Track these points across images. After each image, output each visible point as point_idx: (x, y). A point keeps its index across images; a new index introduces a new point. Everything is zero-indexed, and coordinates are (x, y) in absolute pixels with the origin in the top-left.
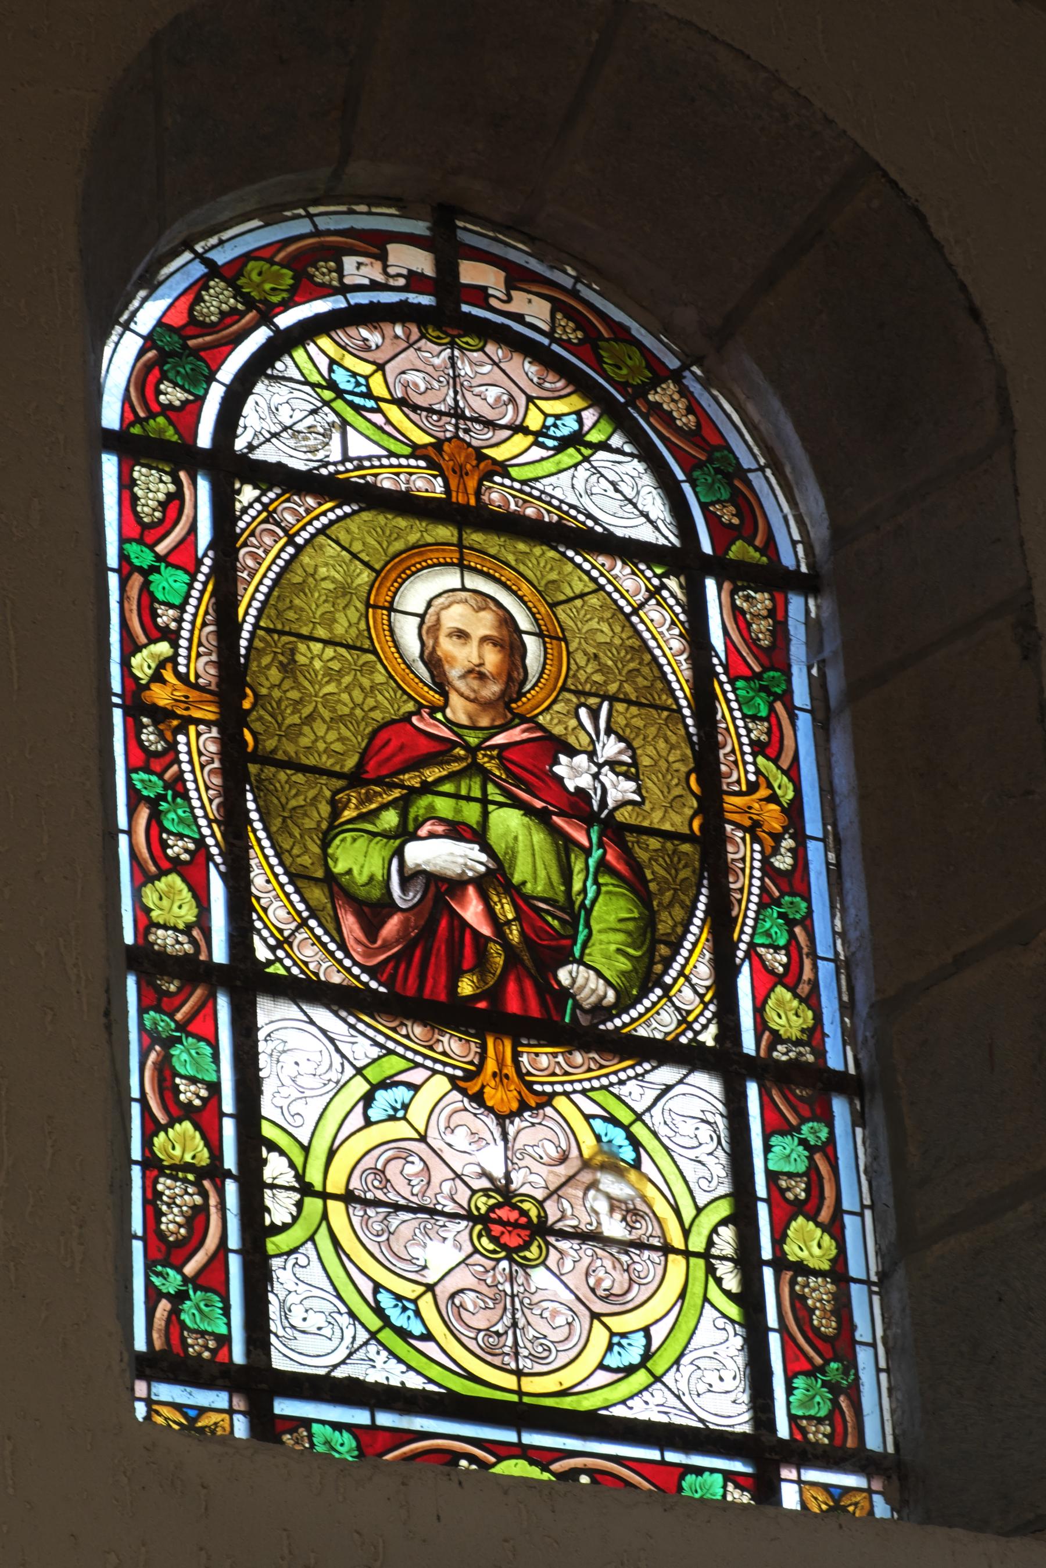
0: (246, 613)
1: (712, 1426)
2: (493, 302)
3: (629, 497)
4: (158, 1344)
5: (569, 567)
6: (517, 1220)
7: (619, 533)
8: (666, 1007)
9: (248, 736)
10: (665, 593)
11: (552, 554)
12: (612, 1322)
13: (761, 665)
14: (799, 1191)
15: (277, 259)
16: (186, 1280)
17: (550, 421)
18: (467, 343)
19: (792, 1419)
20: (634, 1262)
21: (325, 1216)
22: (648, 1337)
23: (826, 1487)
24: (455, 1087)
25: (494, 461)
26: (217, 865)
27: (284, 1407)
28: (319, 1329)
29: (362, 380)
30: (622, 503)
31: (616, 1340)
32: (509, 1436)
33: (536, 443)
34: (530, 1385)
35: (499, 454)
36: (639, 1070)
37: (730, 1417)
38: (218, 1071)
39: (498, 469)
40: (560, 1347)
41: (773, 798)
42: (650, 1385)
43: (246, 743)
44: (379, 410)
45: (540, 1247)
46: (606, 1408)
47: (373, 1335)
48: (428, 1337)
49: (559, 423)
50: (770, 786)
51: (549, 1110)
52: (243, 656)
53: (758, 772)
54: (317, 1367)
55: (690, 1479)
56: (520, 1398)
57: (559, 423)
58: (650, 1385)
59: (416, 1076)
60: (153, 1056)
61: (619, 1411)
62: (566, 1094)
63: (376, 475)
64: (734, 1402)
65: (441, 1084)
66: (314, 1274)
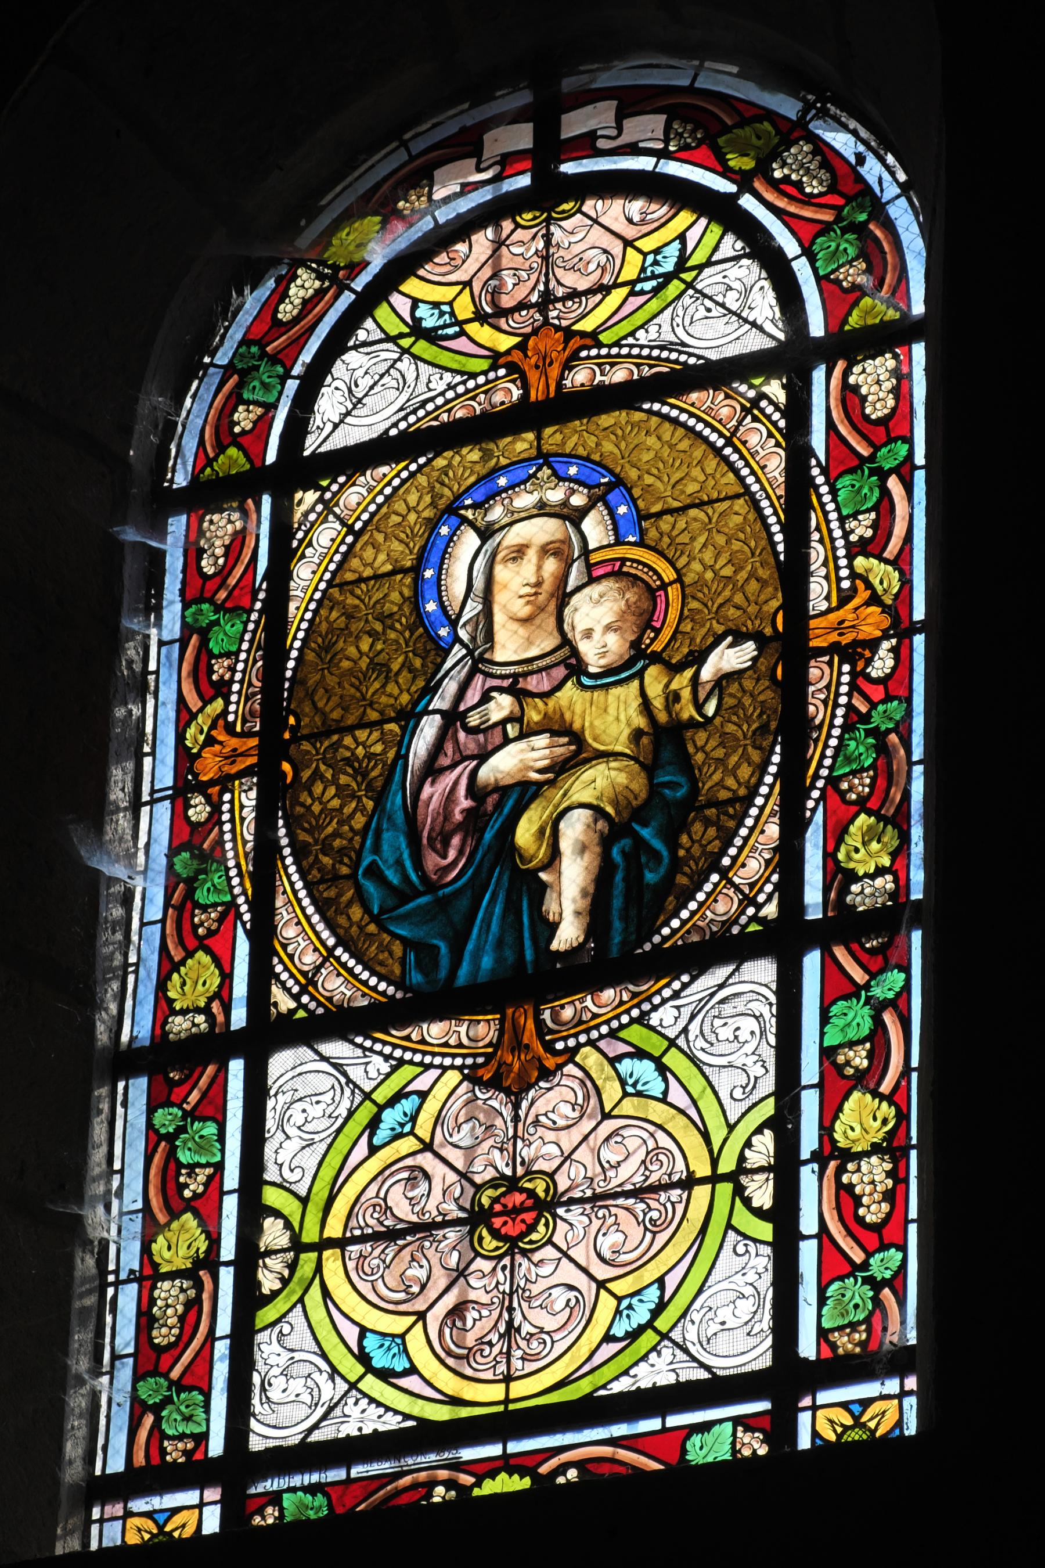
0: (295, 638)
1: (720, 1373)
2: (602, 144)
3: (734, 309)
4: (140, 1459)
5: (655, 420)
6: (522, 1203)
7: (713, 356)
8: (725, 891)
9: (286, 767)
10: (764, 404)
11: (638, 416)
12: (616, 1287)
13: (870, 443)
14: (859, 1058)
15: (211, 455)
16: (171, 1383)
17: (650, 258)
18: (563, 212)
19: (822, 1334)
20: (650, 1209)
21: (319, 1269)
22: (406, 1373)
23: (845, 1405)
24: (465, 1078)
25: (583, 334)
26: (244, 924)
27: (807, 1347)
28: (297, 1395)
29: (446, 308)
30: (726, 319)
31: (622, 1306)
32: (494, 1450)
33: (632, 293)
34: (518, 1389)
35: (587, 325)
36: (676, 985)
37: (743, 1353)
38: (223, 1151)
39: (588, 342)
40: (556, 1337)
41: (875, 599)
42: (658, 1343)
43: (284, 775)
44: (462, 333)
45: (497, 1248)
46: (604, 1387)
47: (353, 1386)
48: (661, 1282)
49: (659, 258)
50: (869, 585)
51: (570, 1069)
52: (289, 680)
53: (854, 576)
54: (292, 1437)
55: (696, 1439)
56: (96, 1521)
57: (659, 258)
58: (658, 1343)
59: (422, 1083)
60: (157, 1159)
61: (617, 1387)
62: (591, 1043)
63: (449, 411)
64: (748, 1334)
65: (453, 1077)
66: (300, 1337)
